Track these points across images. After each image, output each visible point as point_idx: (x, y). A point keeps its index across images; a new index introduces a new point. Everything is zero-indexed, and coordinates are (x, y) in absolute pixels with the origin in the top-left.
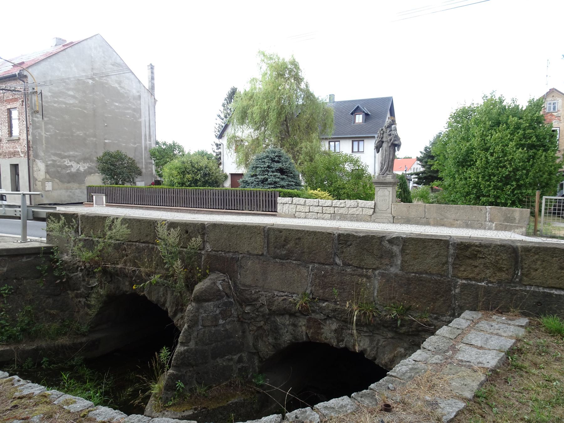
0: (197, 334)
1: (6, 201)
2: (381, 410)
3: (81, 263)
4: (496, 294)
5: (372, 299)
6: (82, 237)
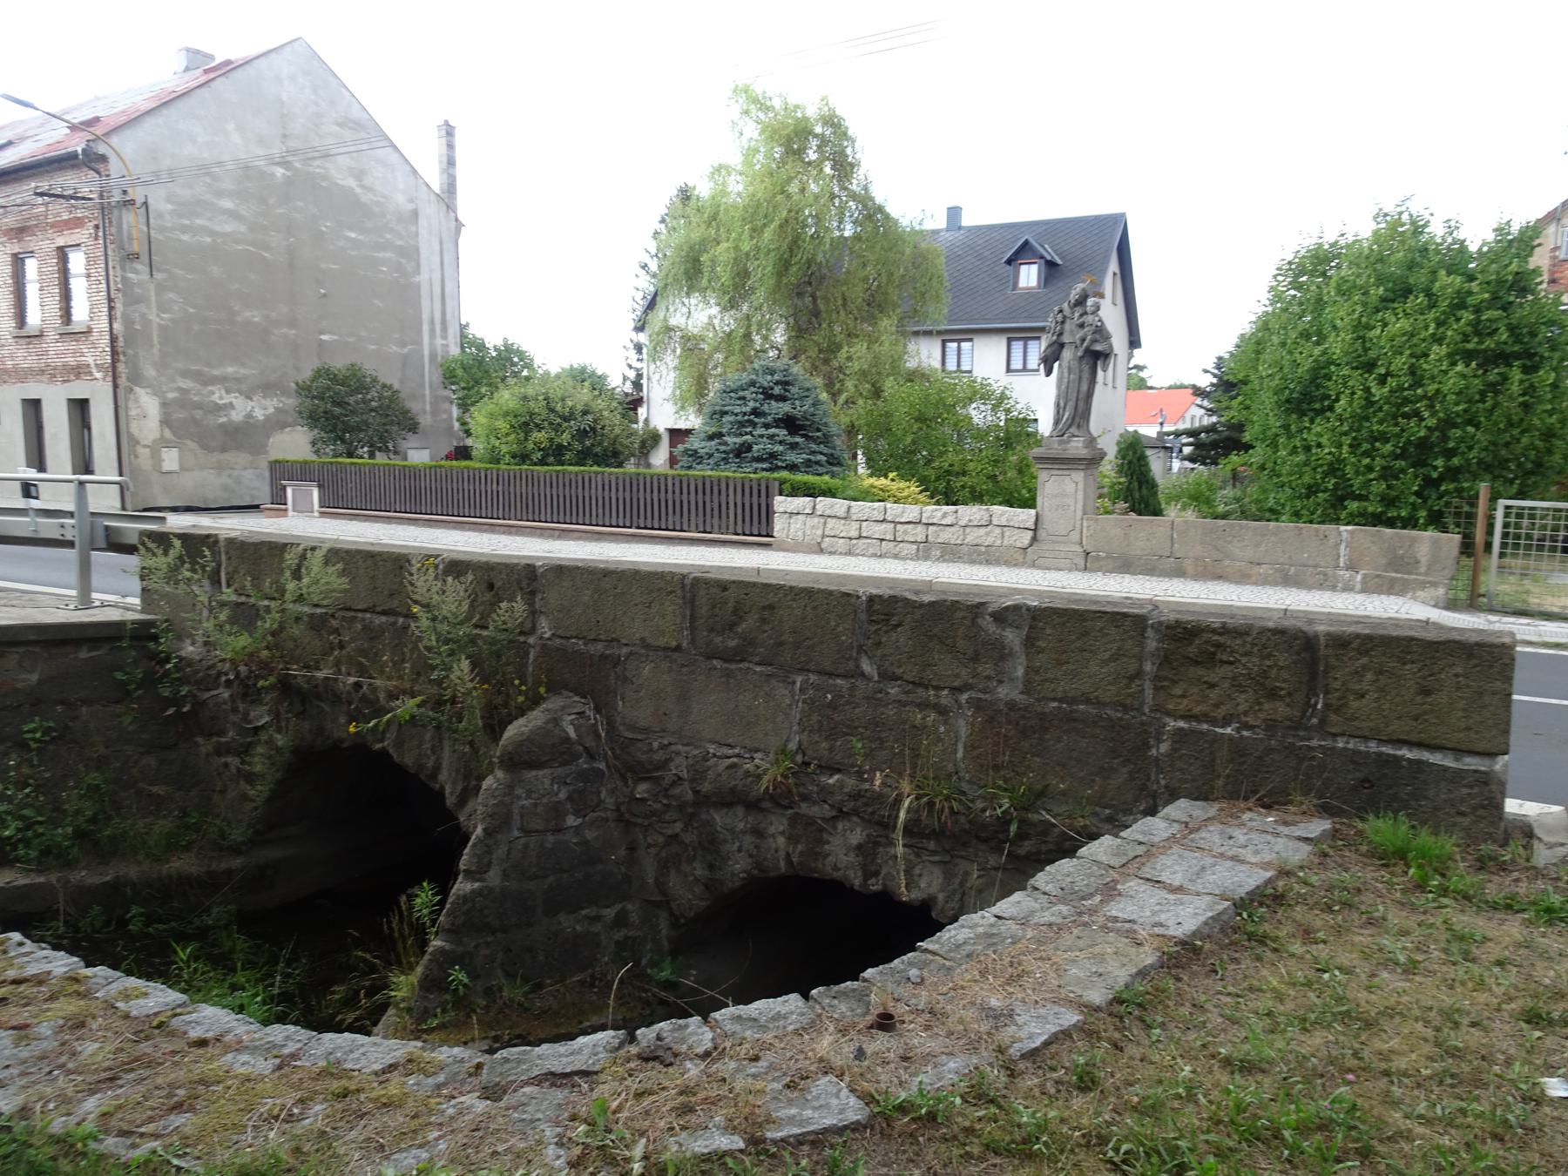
0: (509, 852)
1: (37, 498)
2: (871, 1027)
3: (228, 665)
4: (1260, 758)
5: (951, 768)
6: (228, 594)
